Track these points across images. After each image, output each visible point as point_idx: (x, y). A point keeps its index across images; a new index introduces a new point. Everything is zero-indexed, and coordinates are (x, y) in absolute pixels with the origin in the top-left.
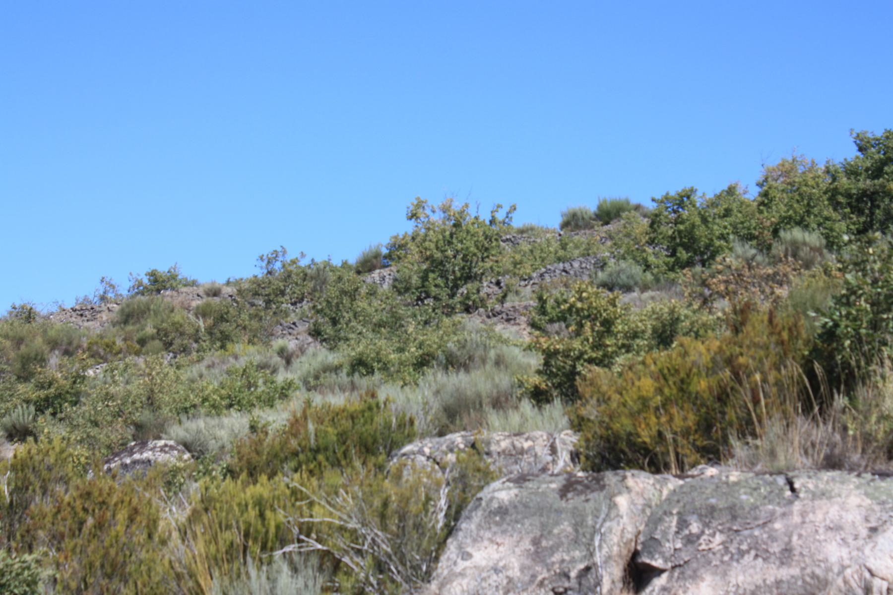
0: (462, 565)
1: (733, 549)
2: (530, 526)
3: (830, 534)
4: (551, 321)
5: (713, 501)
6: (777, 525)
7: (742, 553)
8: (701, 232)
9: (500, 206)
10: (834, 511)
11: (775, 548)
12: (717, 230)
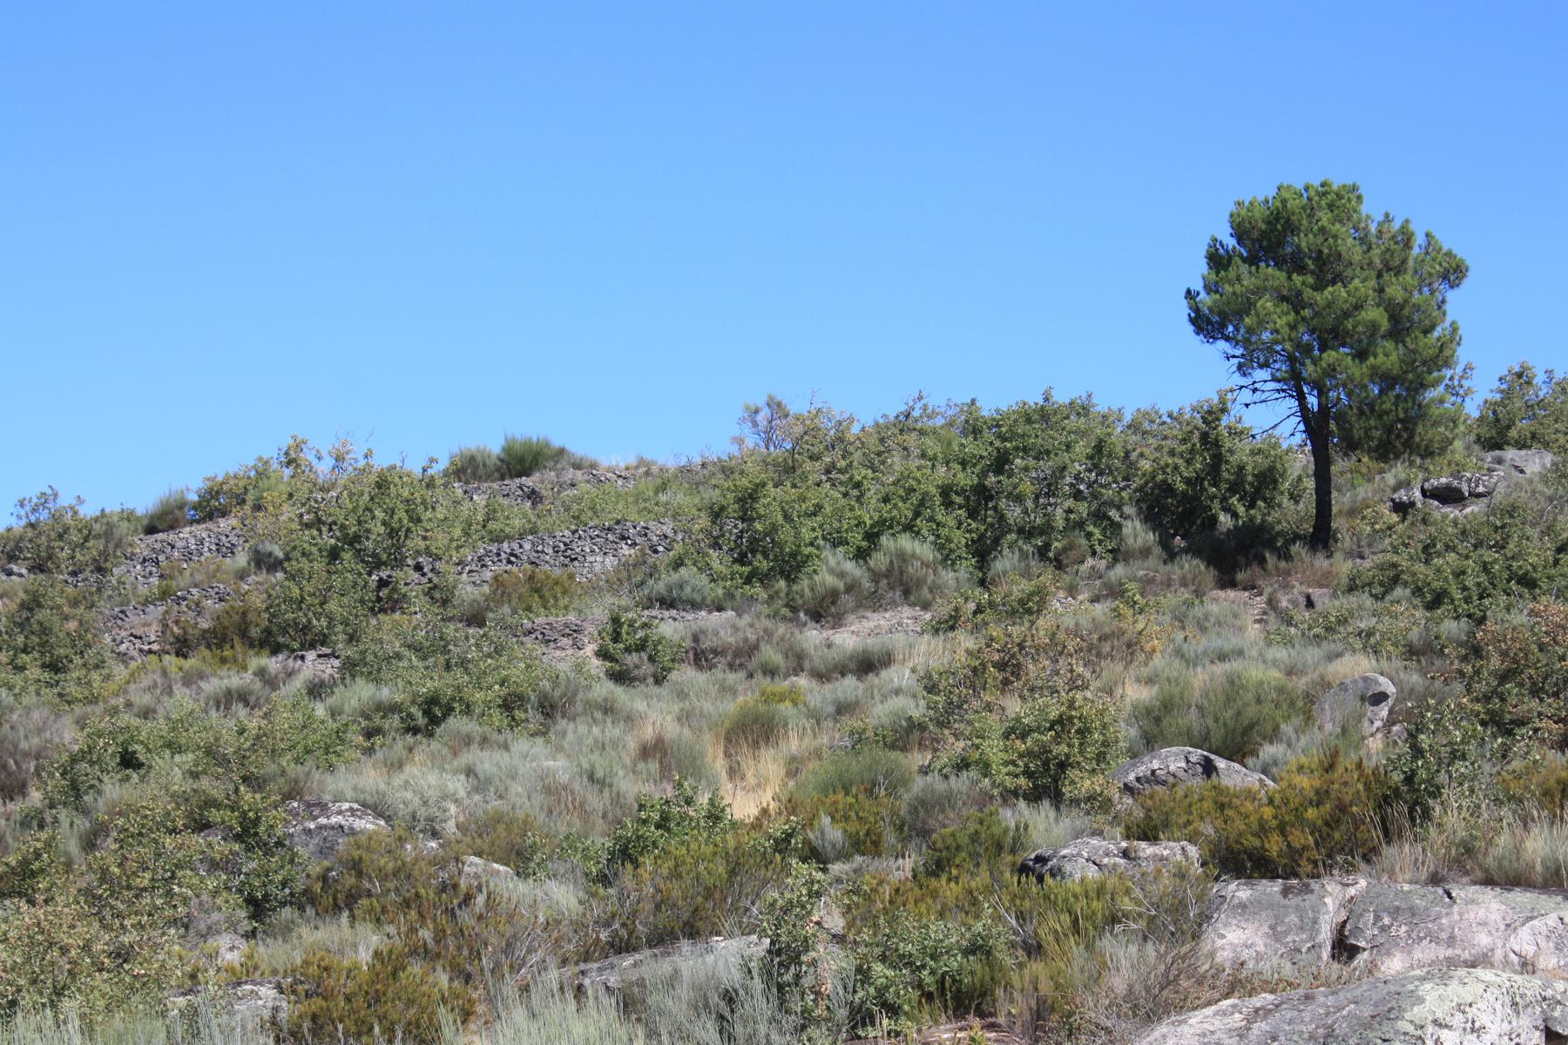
0: (1220, 943)
1: (1414, 935)
3: (1480, 928)
4: (628, 650)
5: (1397, 903)
6: (1444, 921)
7: (1421, 939)
8: (786, 534)
9: (432, 460)
10: (1482, 913)
11: (1444, 936)
12: (807, 535)
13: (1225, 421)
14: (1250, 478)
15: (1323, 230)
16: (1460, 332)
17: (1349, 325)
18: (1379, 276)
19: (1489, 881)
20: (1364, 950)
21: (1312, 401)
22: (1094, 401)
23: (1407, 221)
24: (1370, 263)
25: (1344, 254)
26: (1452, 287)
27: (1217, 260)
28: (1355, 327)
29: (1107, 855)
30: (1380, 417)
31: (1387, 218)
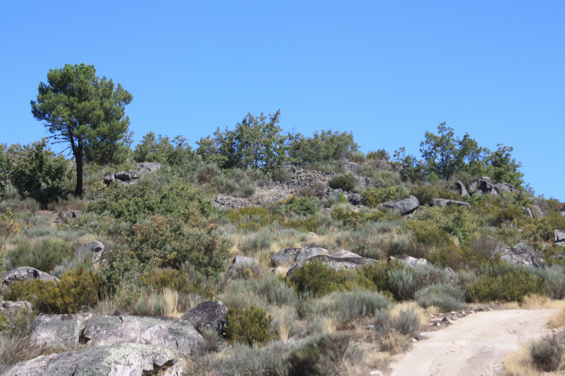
1: (108, 334)
5: (103, 322)
7: (111, 335)
11: (119, 334)
13: (44, 149)
14: (53, 170)
15: (81, 81)
16: (130, 120)
17: (90, 115)
18: (101, 99)
19: (135, 314)
21: (76, 143)
23: (111, 80)
27: (43, 90)
28: (92, 117)
30: (101, 149)
31: (104, 78)
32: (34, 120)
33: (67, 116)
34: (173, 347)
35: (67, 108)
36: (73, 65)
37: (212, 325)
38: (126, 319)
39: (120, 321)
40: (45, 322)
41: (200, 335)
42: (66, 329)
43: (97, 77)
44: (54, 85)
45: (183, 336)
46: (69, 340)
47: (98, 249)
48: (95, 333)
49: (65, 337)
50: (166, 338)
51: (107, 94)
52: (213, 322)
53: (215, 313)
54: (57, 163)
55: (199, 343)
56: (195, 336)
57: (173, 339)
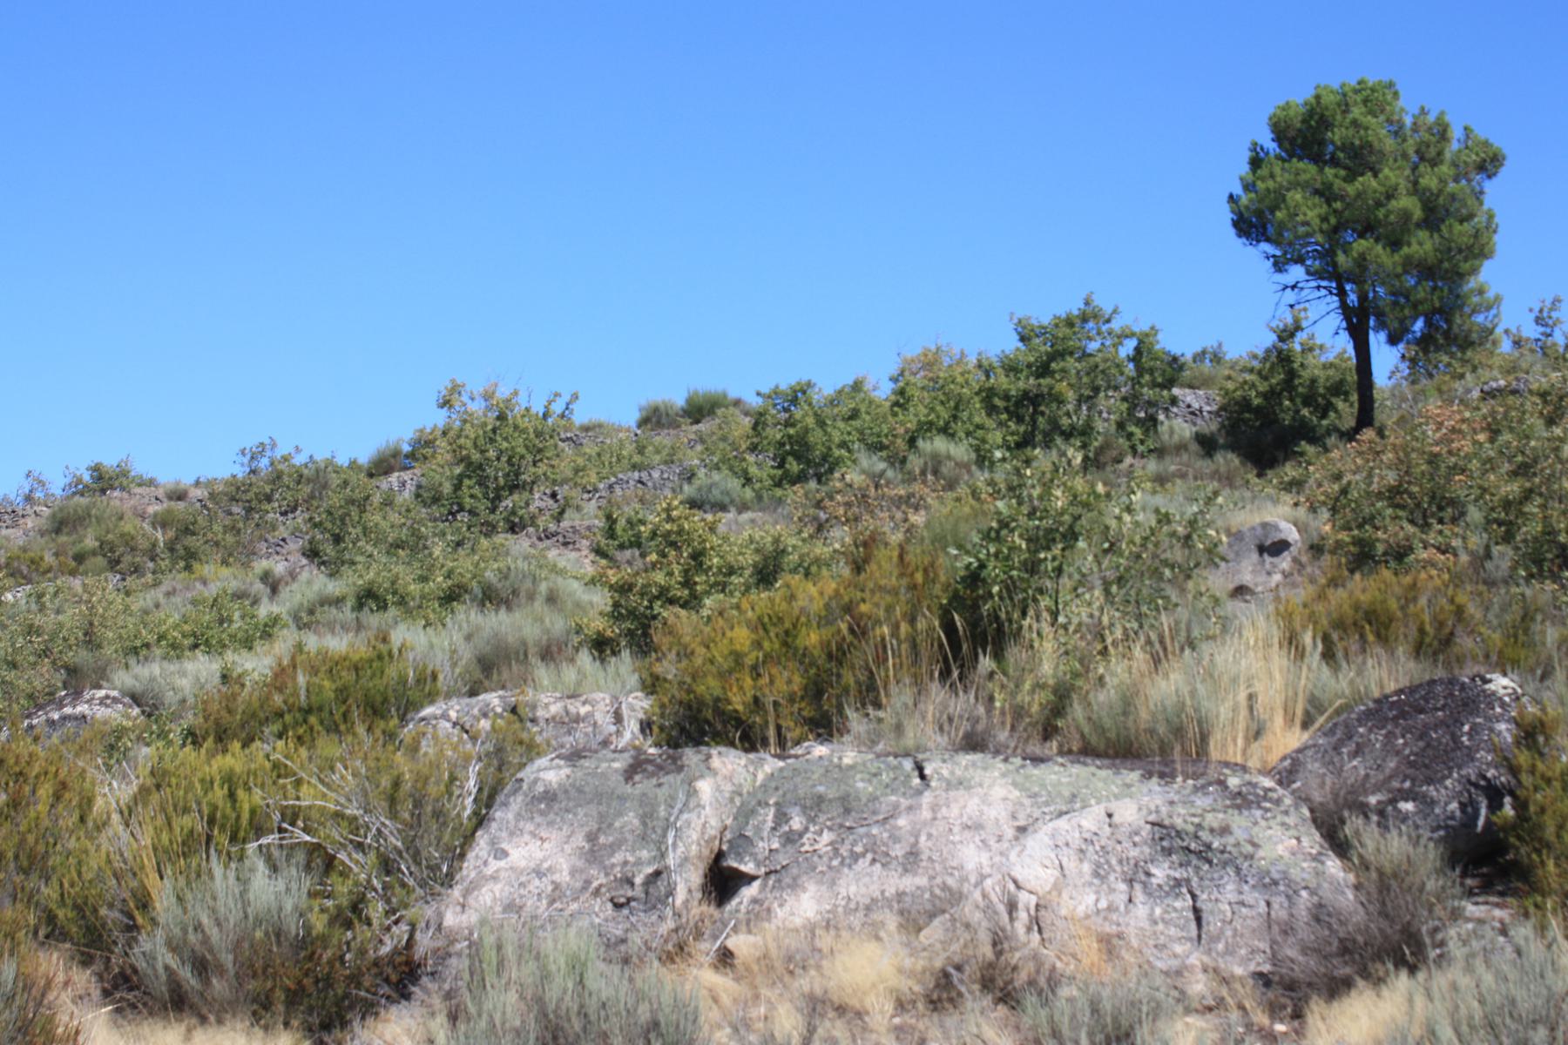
1: (844, 851)
2: (585, 817)
3: (967, 834)
4: (622, 547)
5: (821, 789)
7: (856, 857)
9: (557, 395)
11: (898, 851)
15: (1355, 123)
16: (1496, 220)
17: (1381, 213)
18: (1415, 168)
19: (1088, 752)
20: (753, 878)
21: (1353, 299)
22: (1225, 348)
23: (1442, 113)
24: (1405, 156)
25: (1376, 144)
26: (1489, 177)
28: (1386, 216)
29: (485, 715)
31: (1423, 111)
32: (1237, 244)
33: (1317, 221)
34: (1172, 931)
35: (1317, 199)
36: (1336, 86)
37: (1427, 803)
38: (945, 772)
39: (917, 781)
40: (540, 788)
41: (1333, 865)
42: (636, 822)
43: (1402, 110)
44: (1287, 144)
45: (1231, 871)
46: (638, 880)
47: (1280, 547)
48: (775, 845)
49: (626, 863)
50: (1136, 876)
51: (1432, 152)
52: (1432, 791)
53: (1455, 739)
54: (1331, 372)
55: (1319, 913)
56: (1302, 871)
57: (1178, 883)
